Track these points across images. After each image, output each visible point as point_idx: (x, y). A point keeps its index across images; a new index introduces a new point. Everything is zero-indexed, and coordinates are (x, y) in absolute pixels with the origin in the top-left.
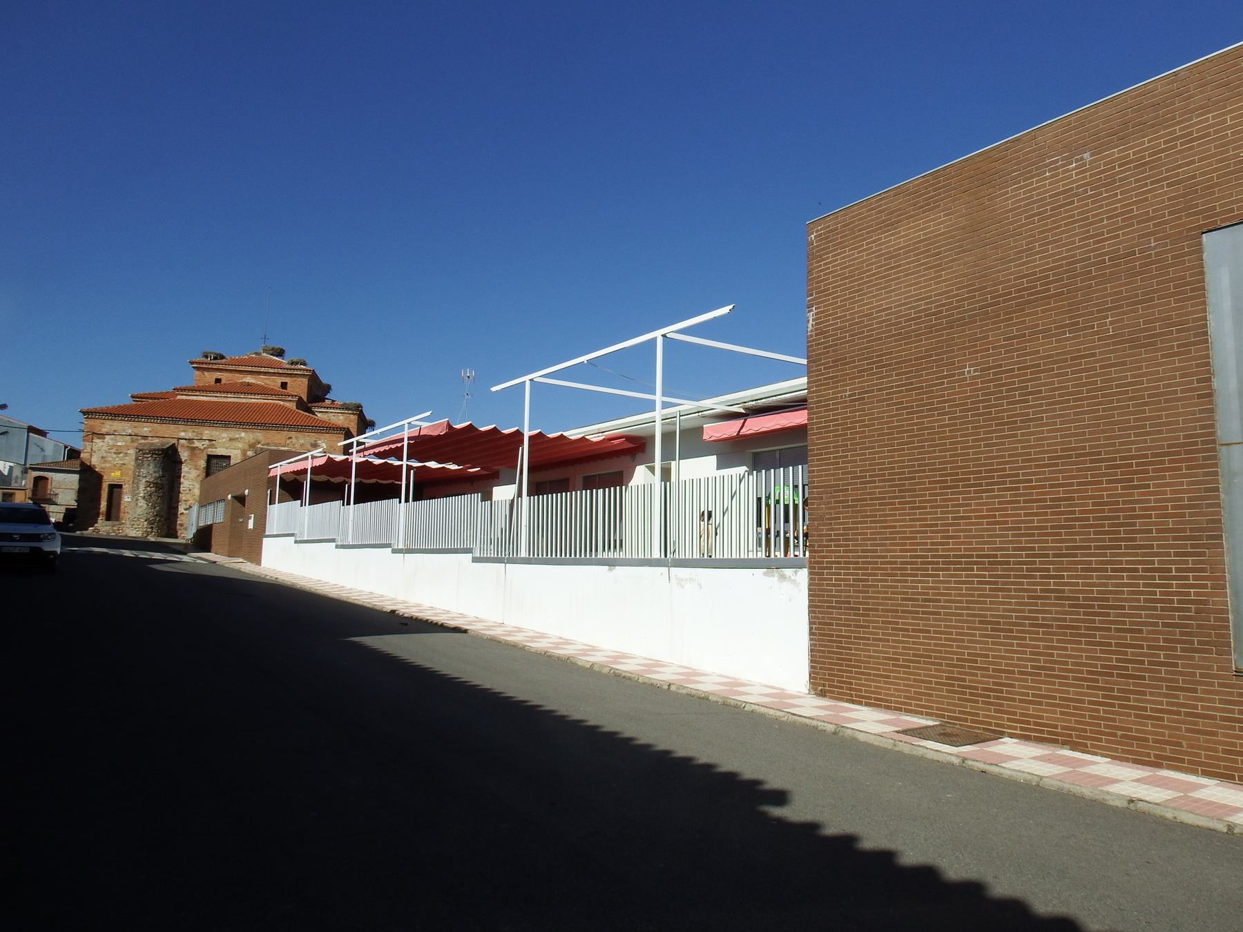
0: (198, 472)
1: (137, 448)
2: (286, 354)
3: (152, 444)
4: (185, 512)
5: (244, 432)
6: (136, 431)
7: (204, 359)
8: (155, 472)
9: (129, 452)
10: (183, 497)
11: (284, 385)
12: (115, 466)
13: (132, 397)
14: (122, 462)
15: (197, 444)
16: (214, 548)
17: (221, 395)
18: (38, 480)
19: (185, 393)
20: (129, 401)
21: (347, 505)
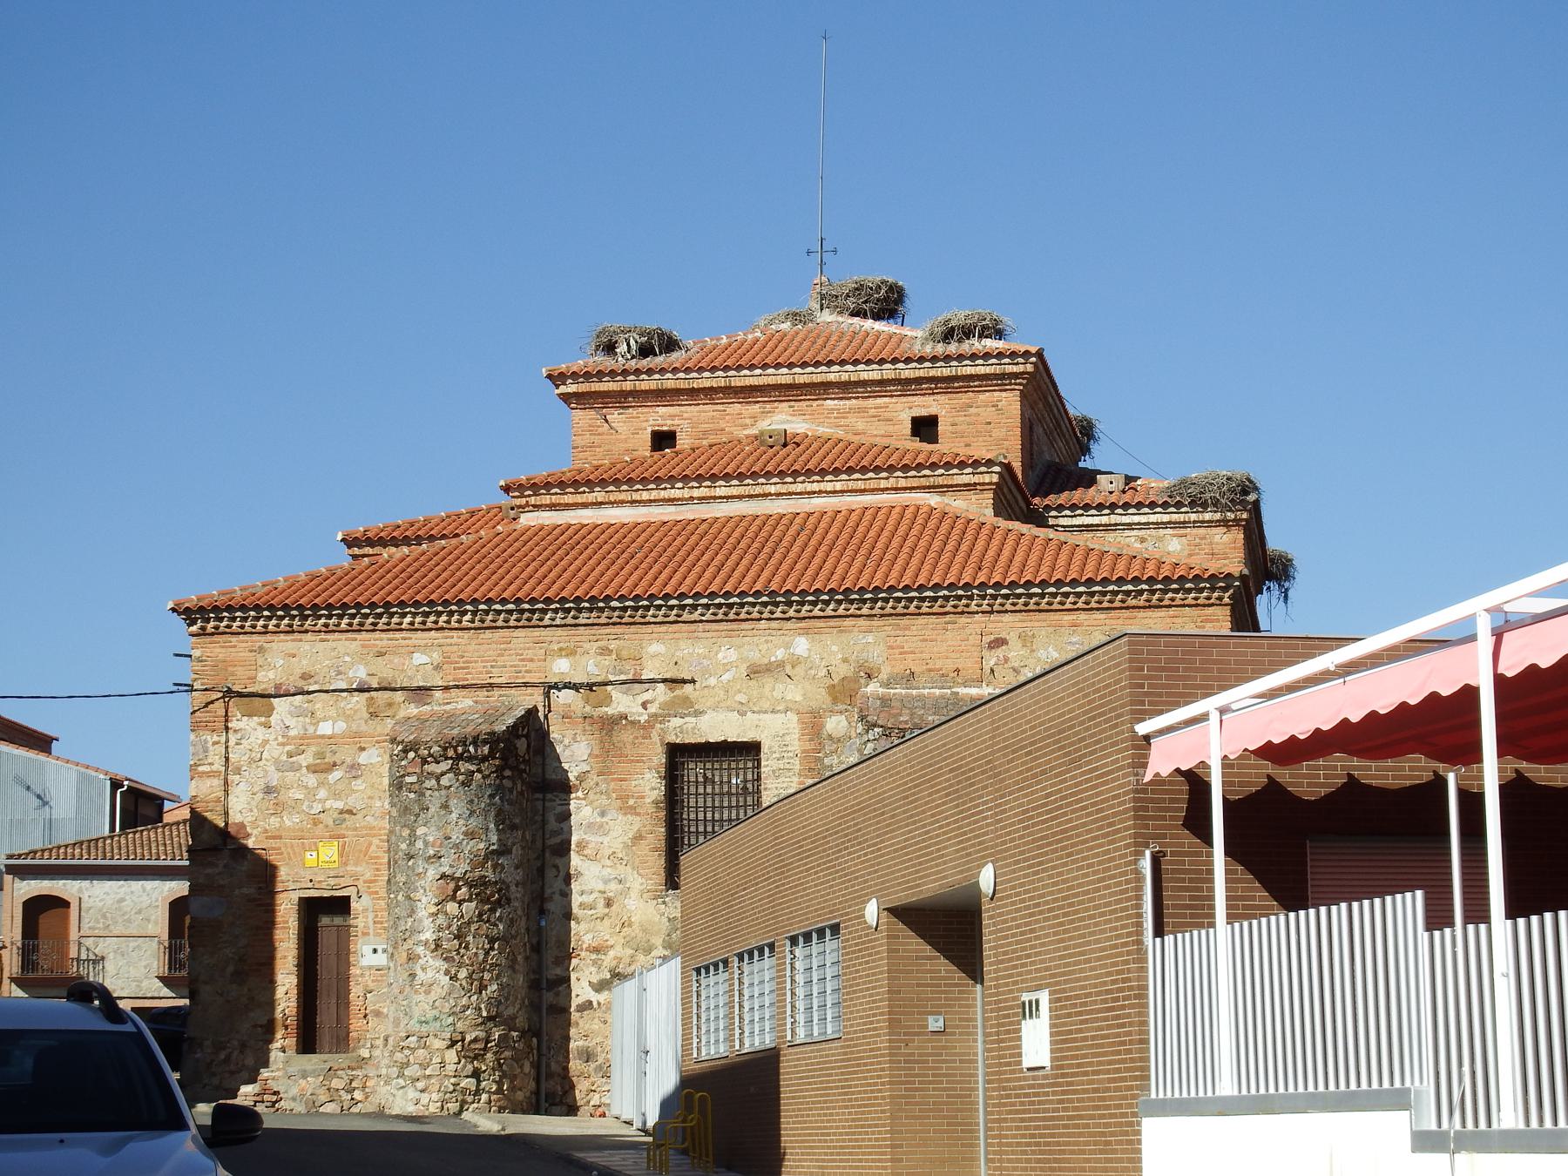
0: (636, 823)
1: (393, 741)
2: (911, 305)
3: (449, 718)
4: (595, 997)
5: (806, 632)
6: (384, 670)
7: (604, 362)
8: (470, 835)
9: (363, 758)
10: (582, 932)
11: (925, 428)
12: (316, 823)
13: (350, 542)
14: (340, 805)
15: (622, 702)
17: (686, 493)
18: (39, 911)
19: (546, 500)
20: (342, 558)
21: (1468, 919)
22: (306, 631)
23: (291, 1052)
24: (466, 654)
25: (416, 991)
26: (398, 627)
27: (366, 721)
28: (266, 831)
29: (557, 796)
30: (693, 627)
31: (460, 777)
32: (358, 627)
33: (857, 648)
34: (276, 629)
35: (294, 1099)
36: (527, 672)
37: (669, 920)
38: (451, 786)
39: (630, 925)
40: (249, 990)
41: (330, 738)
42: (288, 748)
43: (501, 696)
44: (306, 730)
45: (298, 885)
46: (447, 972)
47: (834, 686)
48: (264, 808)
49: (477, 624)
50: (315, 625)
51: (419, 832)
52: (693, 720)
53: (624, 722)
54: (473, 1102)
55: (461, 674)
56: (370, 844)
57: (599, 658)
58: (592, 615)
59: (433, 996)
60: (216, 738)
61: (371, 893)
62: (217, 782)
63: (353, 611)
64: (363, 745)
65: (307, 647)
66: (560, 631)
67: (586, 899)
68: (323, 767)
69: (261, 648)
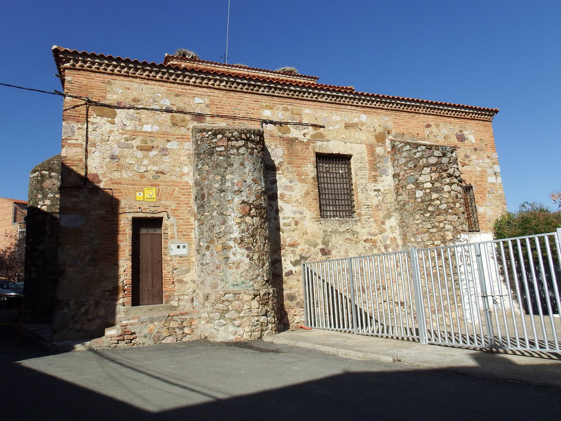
4: (293, 269)
5: (365, 112)
6: (179, 103)
8: (255, 181)
9: (169, 145)
14: (156, 168)
15: (294, 133)
16: (544, 316)
22: (136, 77)
23: (129, 306)
24: (222, 101)
25: (230, 268)
26: (188, 83)
27: (170, 127)
28: (111, 179)
29: (270, 172)
30: (322, 104)
31: (249, 150)
32: (166, 80)
33: (384, 121)
34: (118, 73)
35: (145, 337)
36: (251, 114)
37: (324, 231)
38: (244, 154)
39: (306, 234)
40: (100, 269)
41: (150, 133)
42: (125, 136)
43: (239, 123)
44: (136, 128)
45: (132, 210)
46: (248, 256)
47: (376, 135)
48: (110, 167)
49: (227, 88)
50: (142, 75)
51: (228, 177)
52: (326, 143)
53: (297, 141)
54: (266, 330)
55: (220, 111)
56: (174, 190)
57: (284, 112)
58: (281, 92)
59: (241, 270)
60: (80, 126)
61: (175, 216)
62: (80, 151)
63: (165, 70)
64: (169, 139)
65: (136, 85)
66: (265, 98)
67: (286, 221)
68: (146, 148)
69: (109, 82)
